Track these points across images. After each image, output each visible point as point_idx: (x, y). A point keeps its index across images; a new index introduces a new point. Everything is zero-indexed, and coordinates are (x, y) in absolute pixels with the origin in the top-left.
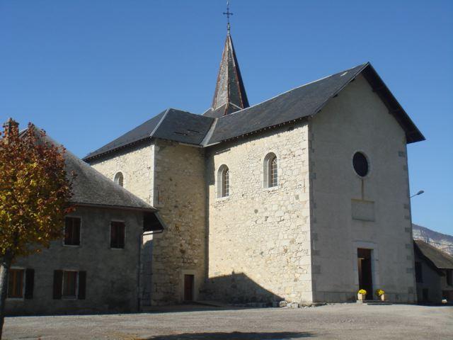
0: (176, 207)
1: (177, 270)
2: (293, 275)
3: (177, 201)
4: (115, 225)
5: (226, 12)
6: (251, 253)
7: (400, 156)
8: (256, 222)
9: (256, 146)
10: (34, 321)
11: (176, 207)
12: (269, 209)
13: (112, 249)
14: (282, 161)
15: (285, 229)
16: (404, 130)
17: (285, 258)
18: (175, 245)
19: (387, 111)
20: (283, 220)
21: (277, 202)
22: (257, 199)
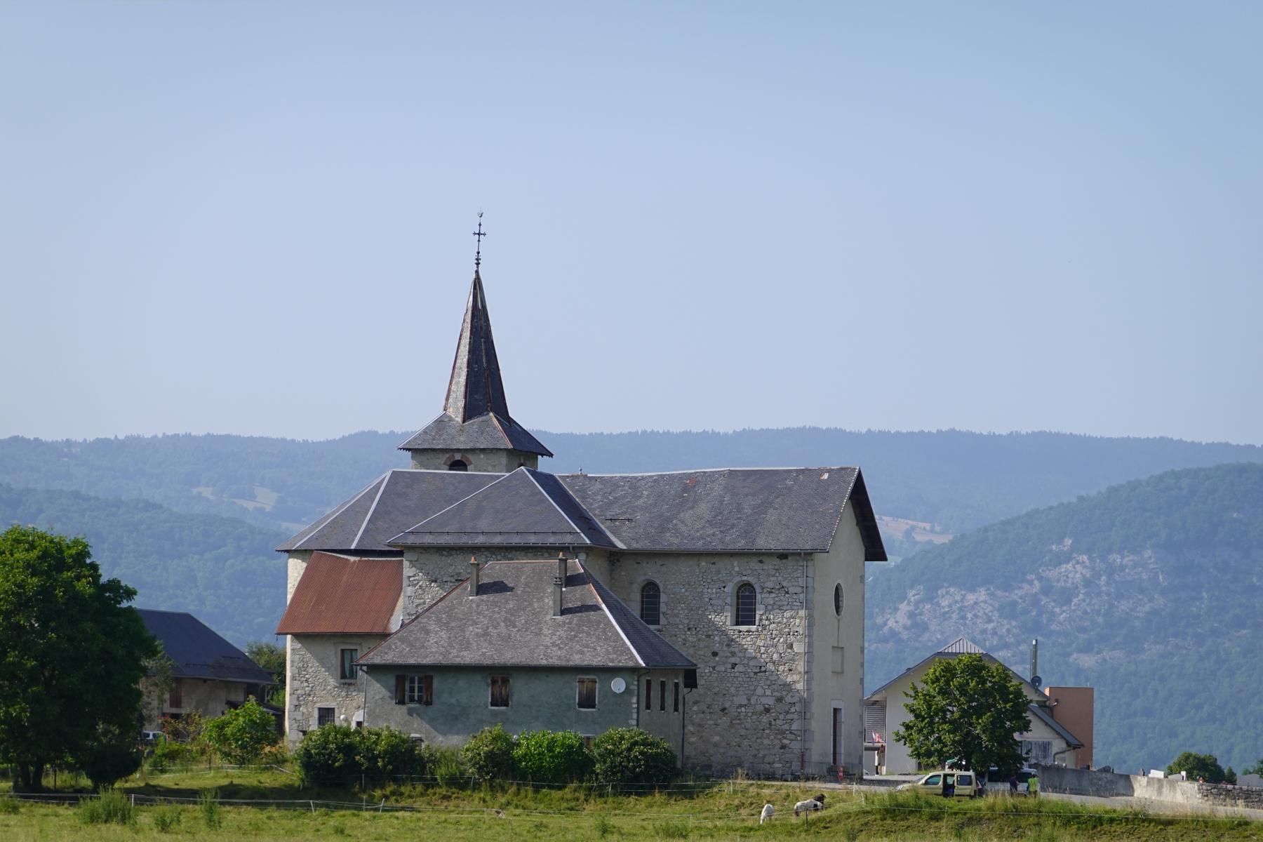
2: (778, 741)
5: (478, 232)
6: (704, 707)
8: (714, 668)
17: (765, 719)
20: (765, 671)
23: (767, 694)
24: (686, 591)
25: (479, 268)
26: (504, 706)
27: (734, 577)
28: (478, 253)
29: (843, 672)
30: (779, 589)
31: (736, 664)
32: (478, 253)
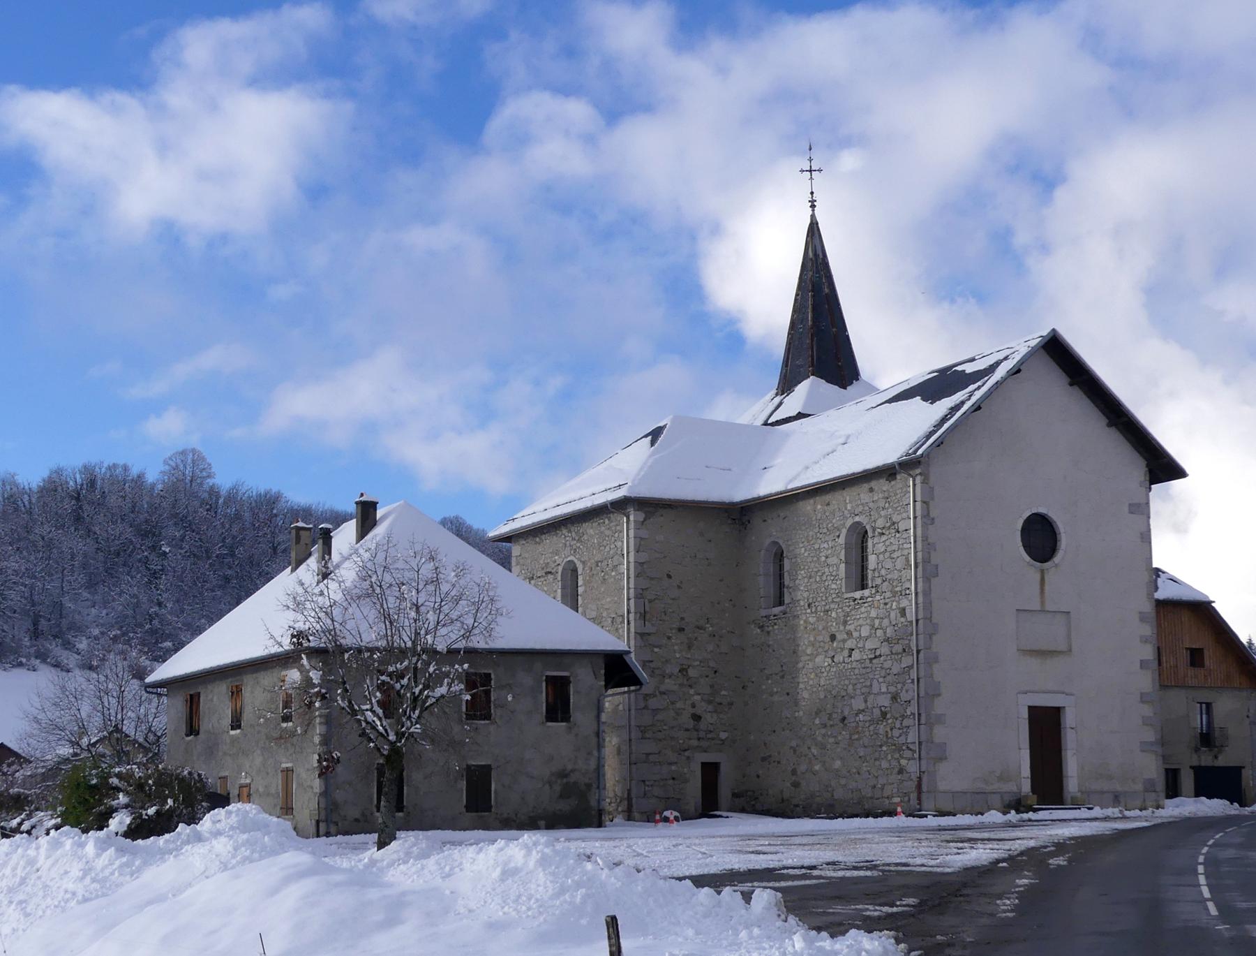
0: (681, 630)
1: (687, 754)
3: (682, 619)
4: (551, 681)
7: (1131, 512)
9: (831, 508)
10: (890, 836)
11: (681, 630)
12: (855, 634)
13: (549, 724)
14: (876, 540)
15: (883, 673)
16: (1145, 458)
17: (882, 728)
18: (679, 705)
19: (1104, 421)
20: (880, 656)
21: (868, 621)
22: (834, 615)
23: (882, 691)
24: (806, 550)
25: (815, 212)
26: (488, 720)
27: (847, 518)
28: (812, 193)
29: (1070, 650)
30: (889, 528)
31: (853, 650)
32: (812, 193)
